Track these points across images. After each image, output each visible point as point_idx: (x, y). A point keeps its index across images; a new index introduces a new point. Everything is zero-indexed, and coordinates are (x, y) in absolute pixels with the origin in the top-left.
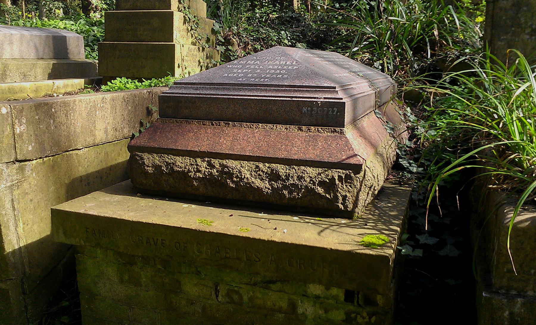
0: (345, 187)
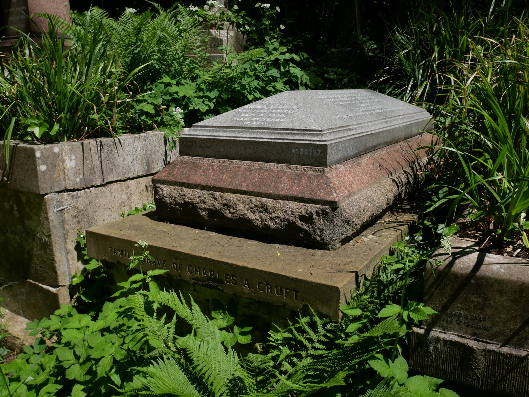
0: (322, 221)
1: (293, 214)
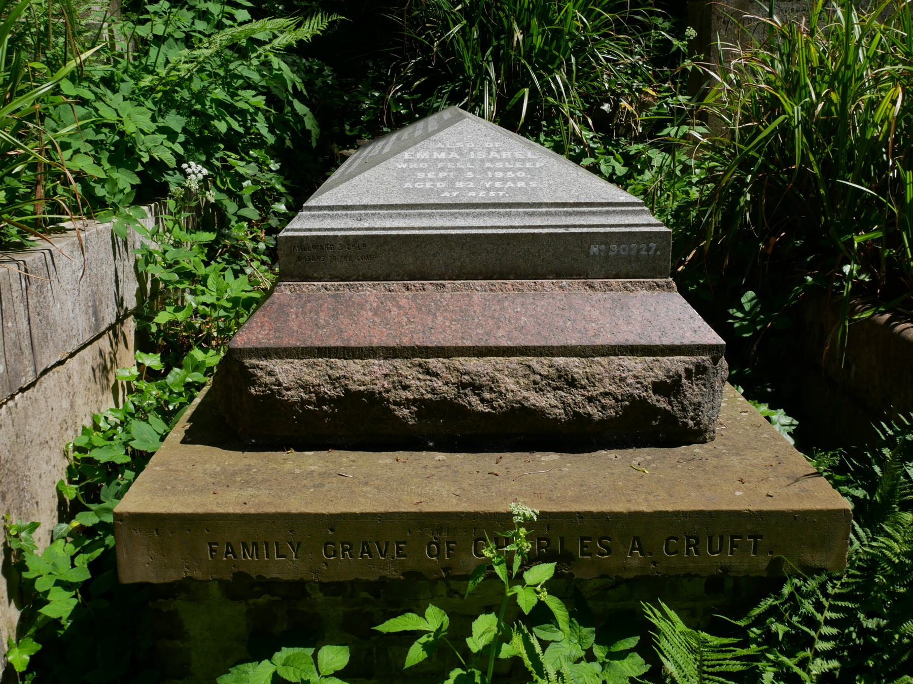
1: (638, 383)
